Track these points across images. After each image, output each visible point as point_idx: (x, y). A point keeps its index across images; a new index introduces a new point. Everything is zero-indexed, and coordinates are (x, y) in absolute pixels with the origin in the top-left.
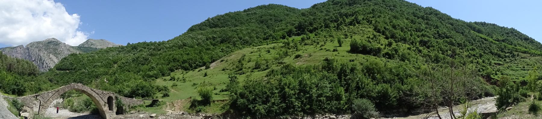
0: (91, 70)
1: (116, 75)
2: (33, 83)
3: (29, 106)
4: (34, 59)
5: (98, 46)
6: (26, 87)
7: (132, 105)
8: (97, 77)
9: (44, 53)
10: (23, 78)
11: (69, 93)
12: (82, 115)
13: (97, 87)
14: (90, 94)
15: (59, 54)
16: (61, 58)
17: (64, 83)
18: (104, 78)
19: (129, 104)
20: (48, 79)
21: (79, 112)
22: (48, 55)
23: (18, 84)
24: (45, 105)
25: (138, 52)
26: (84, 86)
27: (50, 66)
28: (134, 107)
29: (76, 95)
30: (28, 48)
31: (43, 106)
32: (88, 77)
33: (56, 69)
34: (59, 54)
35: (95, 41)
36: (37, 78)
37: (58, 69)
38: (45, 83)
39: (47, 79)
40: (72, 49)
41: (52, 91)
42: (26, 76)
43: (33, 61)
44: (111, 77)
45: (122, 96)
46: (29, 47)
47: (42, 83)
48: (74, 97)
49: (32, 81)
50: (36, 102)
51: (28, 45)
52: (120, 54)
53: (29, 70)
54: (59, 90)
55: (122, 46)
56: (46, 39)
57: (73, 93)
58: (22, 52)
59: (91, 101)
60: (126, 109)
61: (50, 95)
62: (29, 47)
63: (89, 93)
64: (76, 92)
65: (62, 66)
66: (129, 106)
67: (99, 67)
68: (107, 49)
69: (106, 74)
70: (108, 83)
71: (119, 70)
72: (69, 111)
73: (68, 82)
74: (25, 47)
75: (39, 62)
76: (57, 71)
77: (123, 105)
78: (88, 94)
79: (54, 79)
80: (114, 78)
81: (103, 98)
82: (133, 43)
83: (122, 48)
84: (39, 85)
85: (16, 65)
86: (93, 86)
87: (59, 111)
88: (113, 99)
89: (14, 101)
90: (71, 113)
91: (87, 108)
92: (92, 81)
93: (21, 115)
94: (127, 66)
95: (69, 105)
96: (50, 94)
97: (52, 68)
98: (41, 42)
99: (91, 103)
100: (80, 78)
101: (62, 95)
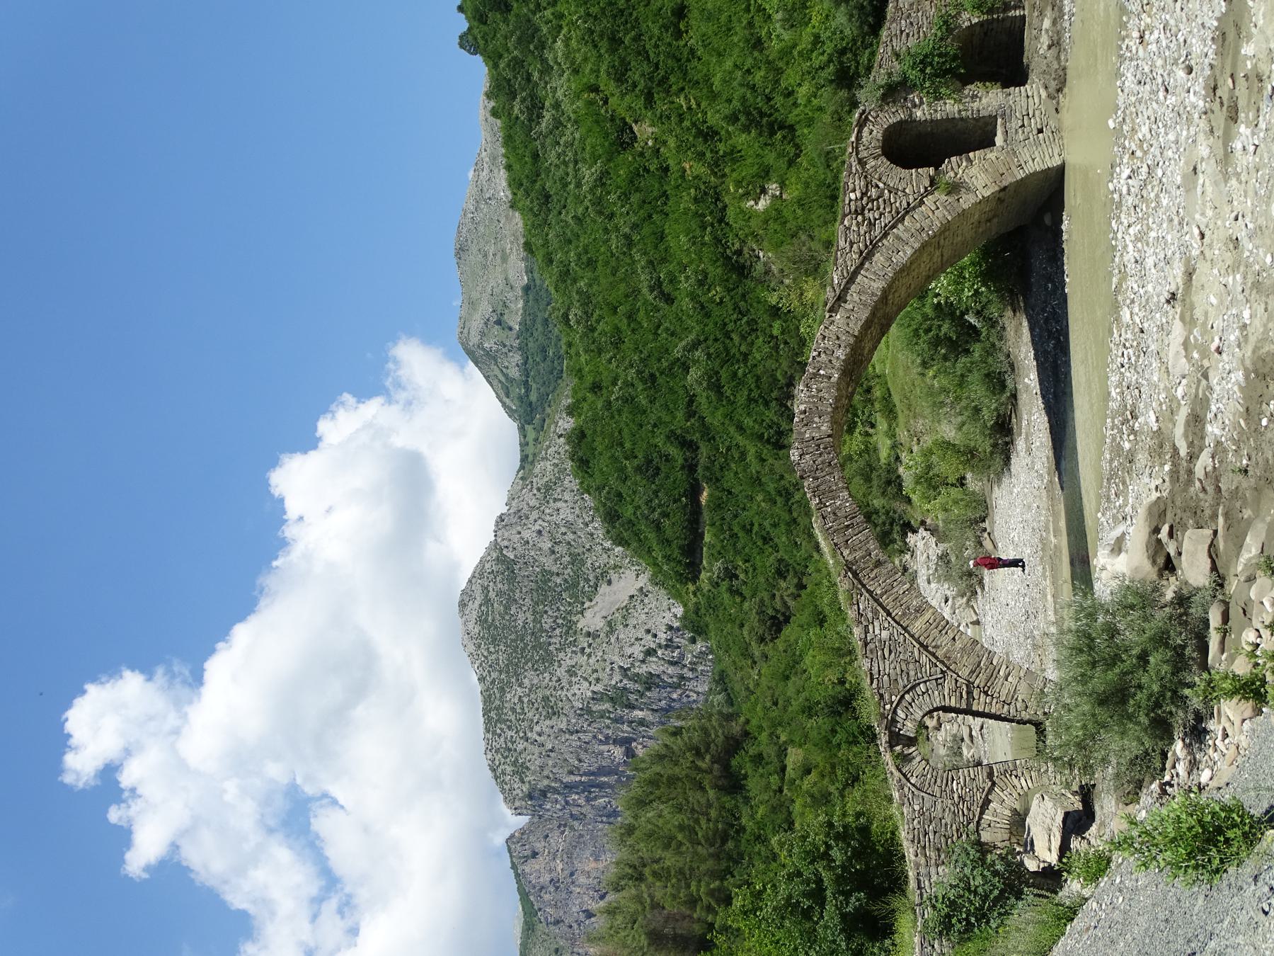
1: (714, 119)
2: (794, 757)
3: (979, 797)
5: (511, 274)
6: (830, 825)
9: (571, 672)
11: (868, 479)
12: (1033, 376)
13: (814, 269)
14: (873, 314)
15: (577, 560)
16: (608, 544)
17: (794, 520)
18: (748, 216)
21: (1014, 396)
22: (583, 642)
23: (806, 895)
24: (964, 672)
26: (810, 369)
27: (670, 628)
29: (882, 425)
30: (530, 797)
31: (969, 684)
32: (743, 338)
33: (691, 587)
34: (577, 560)
35: (472, 304)
36: (761, 728)
37: (691, 570)
38: (792, 667)
39: (768, 648)
40: (537, 469)
41: (851, 614)
42: (746, 811)
43: (630, 753)
44: (734, 156)
45: (873, 54)
46: (525, 788)
48: (894, 447)
49: (784, 769)
51: (510, 799)
53: (702, 789)
54: (849, 566)
55: (489, 96)
57: (869, 450)
58: (558, 841)
61: (885, 634)
62: (521, 789)
63: (868, 325)
64: (859, 428)
65: (669, 542)
69: (712, 198)
70: (783, 185)
71: (681, 101)
72: (1005, 480)
73: (786, 494)
75: (639, 714)
76: (704, 575)
78: (874, 330)
79: (766, 596)
80: (741, 139)
83: (502, 90)
84: (809, 710)
85: (658, 895)
86: (809, 295)
87: (1007, 554)
88: (901, 122)
89: (946, 926)
90: (1019, 461)
92: (775, 312)
93: (1053, 858)
94: (637, 38)
95: (961, 481)
97: (679, 611)
98: (487, 700)
101: (885, 540)
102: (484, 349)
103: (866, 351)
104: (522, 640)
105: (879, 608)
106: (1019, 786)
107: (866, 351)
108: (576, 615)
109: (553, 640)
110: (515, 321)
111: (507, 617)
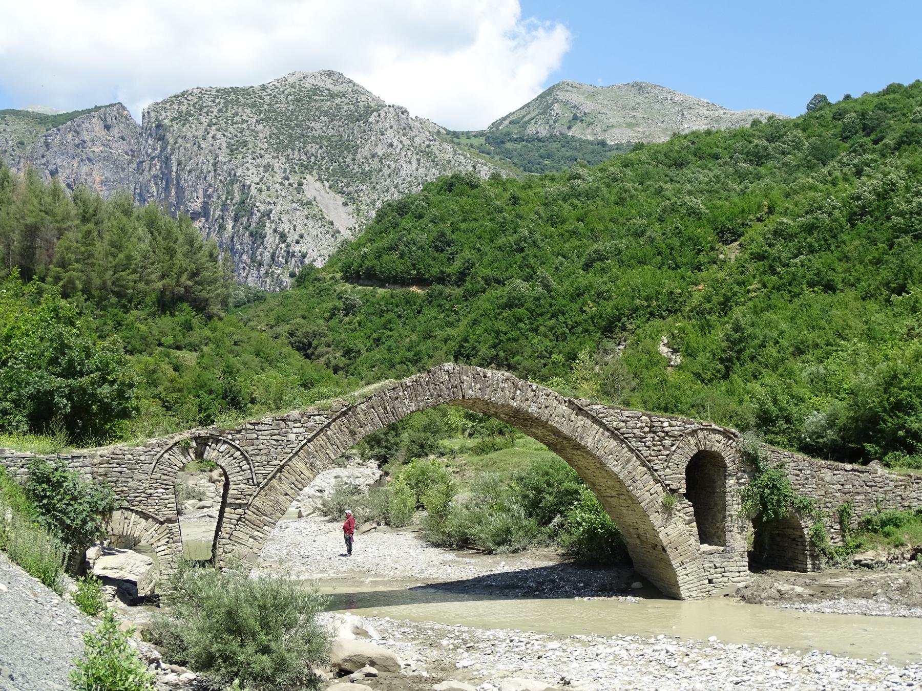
0: (567, 283)
2: (189, 358)
3: (150, 511)
4: (196, 205)
5: (616, 131)
6: (131, 386)
7: (862, 511)
8: (609, 330)
10: (119, 324)
11: (426, 429)
13: (607, 391)
14: (565, 437)
15: (366, 176)
16: (379, 204)
18: (655, 337)
19: (840, 504)
20: (291, 334)
21: (490, 553)
22: (294, 179)
23: (71, 361)
24: (258, 502)
25: (883, 156)
26: (521, 382)
28: (884, 524)
30: (159, 126)
31: (247, 506)
32: (551, 329)
33: (338, 275)
34: (366, 176)
35: (592, 95)
36: (215, 330)
37: (353, 276)
38: (266, 359)
39: (283, 339)
41: (311, 409)
43: (195, 216)
44: (706, 328)
46: (167, 122)
47: (245, 364)
48: (452, 452)
49: (179, 348)
50: (201, 482)
51: (158, 108)
52: (759, 177)
53: (163, 277)
54: (351, 409)
56: (281, 76)
57: (451, 431)
58: (119, 149)
59: (566, 485)
60: (821, 539)
62: (166, 118)
63: (556, 432)
66: (843, 516)
67: (621, 263)
68: (671, 142)
70: (679, 367)
73: (416, 361)
74: (139, 120)
75: (230, 225)
76: (348, 286)
77: (803, 508)
78: (552, 438)
79: (329, 339)
80: (719, 334)
81: (657, 464)
82: (848, 97)
84: (229, 371)
85: (70, 235)
86: (585, 386)
89: (43, 479)
90: (435, 554)
91: (546, 521)
92: (572, 357)
95: (420, 507)
96: (295, 433)
97: (319, 264)
98: (245, 92)
99: (573, 494)
100: (498, 333)
101: (373, 441)
102: (552, 103)
103: (534, 430)
104: (297, 125)
105: (315, 432)
106: (159, 544)
107: (534, 430)
108: (318, 173)
109: (296, 153)
110: (576, 132)
111: (317, 113)
